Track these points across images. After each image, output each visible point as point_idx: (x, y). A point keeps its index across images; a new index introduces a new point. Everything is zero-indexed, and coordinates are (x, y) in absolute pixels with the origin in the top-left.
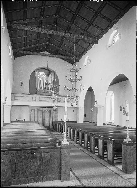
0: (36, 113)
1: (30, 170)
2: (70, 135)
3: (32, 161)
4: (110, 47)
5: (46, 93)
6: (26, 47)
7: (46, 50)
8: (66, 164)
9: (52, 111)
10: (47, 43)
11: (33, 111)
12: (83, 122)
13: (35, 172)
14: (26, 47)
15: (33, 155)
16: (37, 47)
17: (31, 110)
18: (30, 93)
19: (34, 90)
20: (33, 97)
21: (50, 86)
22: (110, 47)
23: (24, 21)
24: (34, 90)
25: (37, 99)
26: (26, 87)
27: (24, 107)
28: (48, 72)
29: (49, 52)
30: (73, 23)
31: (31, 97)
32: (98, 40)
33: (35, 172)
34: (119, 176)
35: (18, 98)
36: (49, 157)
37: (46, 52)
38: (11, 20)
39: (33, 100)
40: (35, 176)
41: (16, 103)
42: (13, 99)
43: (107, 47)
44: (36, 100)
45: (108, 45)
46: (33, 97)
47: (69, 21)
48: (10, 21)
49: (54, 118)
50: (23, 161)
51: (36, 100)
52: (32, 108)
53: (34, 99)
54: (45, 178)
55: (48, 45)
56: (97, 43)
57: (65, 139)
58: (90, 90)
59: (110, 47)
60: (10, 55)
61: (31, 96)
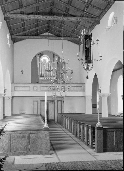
0: (39, 104)
1: (21, 146)
2: (71, 128)
3: (22, 140)
4: (109, 28)
5: (47, 82)
6: (25, 32)
7: (47, 31)
8: (46, 142)
9: (56, 102)
10: (47, 25)
11: (35, 103)
12: (91, 113)
13: (24, 147)
14: (25, 32)
15: (23, 135)
16: (37, 30)
17: (34, 101)
18: (32, 83)
19: (35, 79)
20: (34, 87)
21: (53, 73)
22: (109, 28)
23: (20, 10)
24: (35, 79)
25: (39, 89)
26: (27, 76)
27: (26, 97)
28: (53, 55)
29: (50, 33)
30: (70, 5)
31: (32, 87)
32: (99, 21)
33: (24, 147)
34: (91, 154)
35: (18, 89)
36: (35, 137)
37: (47, 34)
38: (8, 11)
39: (34, 90)
40: (25, 150)
41: (16, 94)
42: (13, 90)
43: (107, 29)
44: (37, 90)
45: (107, 27)
46: (34, 87)
47: (66, 3)
48: (6, 12)
49: (59, 110)
50: (16, 139)
51: (37, 90)
52: (35, 99)
53: (35, 88)
54: (32, 153)
55: (49, 27)
56: (98, 23)
57: (46, 123)
58: (96, 75)
59: (110, 29)
60: (8, 43)
61: (32, 86)
